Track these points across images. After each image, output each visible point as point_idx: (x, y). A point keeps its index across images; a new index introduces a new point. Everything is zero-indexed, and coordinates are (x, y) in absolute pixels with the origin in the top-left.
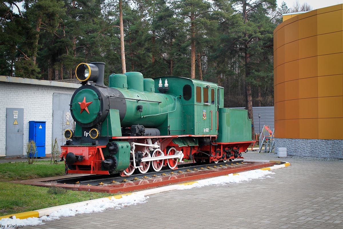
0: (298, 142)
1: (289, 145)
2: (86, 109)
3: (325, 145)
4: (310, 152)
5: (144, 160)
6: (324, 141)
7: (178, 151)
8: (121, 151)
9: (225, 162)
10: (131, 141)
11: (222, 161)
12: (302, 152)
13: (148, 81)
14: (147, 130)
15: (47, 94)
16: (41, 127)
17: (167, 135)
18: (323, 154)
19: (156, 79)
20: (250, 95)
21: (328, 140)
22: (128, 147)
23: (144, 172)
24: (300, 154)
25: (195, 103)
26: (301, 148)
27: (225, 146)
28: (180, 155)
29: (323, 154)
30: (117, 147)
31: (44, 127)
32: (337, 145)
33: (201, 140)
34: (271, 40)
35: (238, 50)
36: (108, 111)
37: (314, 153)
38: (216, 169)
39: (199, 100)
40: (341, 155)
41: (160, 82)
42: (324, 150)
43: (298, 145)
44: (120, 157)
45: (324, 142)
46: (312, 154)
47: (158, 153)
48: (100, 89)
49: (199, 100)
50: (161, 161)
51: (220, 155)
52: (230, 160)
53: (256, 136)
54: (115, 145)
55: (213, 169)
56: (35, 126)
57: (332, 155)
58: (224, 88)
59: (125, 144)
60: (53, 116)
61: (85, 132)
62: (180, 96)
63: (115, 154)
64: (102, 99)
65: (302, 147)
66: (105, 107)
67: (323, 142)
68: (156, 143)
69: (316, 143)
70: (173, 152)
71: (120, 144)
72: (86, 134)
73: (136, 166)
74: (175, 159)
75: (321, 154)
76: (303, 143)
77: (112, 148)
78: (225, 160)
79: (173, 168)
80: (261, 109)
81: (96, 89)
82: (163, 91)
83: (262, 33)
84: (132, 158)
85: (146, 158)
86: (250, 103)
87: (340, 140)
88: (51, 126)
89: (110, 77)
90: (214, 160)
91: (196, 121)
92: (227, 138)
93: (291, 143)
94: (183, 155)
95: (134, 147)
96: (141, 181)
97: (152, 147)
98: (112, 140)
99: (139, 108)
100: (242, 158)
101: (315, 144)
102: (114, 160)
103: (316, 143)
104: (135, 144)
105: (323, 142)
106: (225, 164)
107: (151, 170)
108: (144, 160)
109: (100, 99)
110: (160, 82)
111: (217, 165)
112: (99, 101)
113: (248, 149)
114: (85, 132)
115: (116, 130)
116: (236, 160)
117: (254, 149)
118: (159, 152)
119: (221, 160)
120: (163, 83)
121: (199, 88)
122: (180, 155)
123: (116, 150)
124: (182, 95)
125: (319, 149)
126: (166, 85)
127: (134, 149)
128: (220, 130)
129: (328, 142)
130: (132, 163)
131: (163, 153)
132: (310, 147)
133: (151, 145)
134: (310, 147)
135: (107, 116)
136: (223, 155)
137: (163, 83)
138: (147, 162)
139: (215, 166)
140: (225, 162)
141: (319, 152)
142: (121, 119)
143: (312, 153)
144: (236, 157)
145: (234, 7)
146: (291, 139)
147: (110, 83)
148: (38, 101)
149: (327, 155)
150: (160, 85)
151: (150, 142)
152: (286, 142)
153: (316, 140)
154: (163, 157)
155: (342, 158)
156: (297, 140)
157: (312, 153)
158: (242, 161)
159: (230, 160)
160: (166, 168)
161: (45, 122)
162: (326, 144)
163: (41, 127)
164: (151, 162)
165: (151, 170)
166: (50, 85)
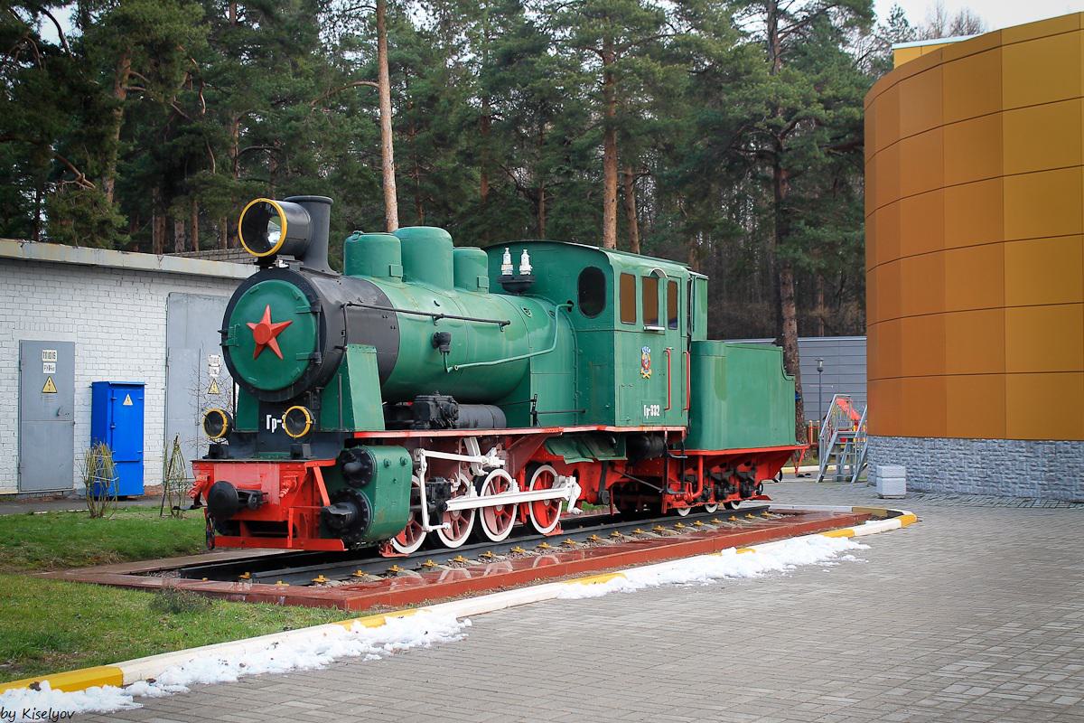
0: (941, 449)
1: (913, 458)
2: (273, 343)
3: (1028, 459)
4: (978, 479)
5: (455, 505)
6: (1024, 444)
7: (562, 478)
8: (382, 477)
9: (711, 510)
10: (412, 444)
11: (703, 509)
12: (956, 480)
13: (468, 257)
14: (465, 412)
15: (149, 297)
16: (128, 402)
17: (527, 425)
18: (1022, 485)
19: (494, 249)
20: (791, 298)
21: (1037, 441)
22: (403, 463)
23: (455, 544)
24: (948, 486)
25: (618, 325)
26: (950, 468)
27: (711, 461)
28: (569, 490)
29: (1022, 485)
30: (370, 465)
31: (139, 402)
32: (1066, 457)
33: (634, 442)
34: (858, 127)
35: (753, 159)
36: (340, 351)
37: (991, 484)
38: (683, 533)
39: (628, 316)
40: (1077, 490)
41: (507, 258)
42: (1024, 473)
43: (941, 458)
44: (380, 496)
45: (1024, 450)
46: (986, 486)
47: (500, 484)
48: (316, 281)
49: (628, 316)
50: (508, 508)
51: (695, 491)
52: (728, 506)
53: (808, 428)
54: (365, 458)
55: (674, 534)
56: (109, 397)
57: (1050, 489)
58: (706, 277)
59: (395, 456)
60: (167, 366)
61: (270, 416)
62: (570, 302)
63: (362, 486)
64: (322, 313)
65: (954, 465)
66: (333, 338)
67: (1020, 450)
68: (494, 451)
69: (998, 453)
70: (547, 481)
71: (379, 456)
72: (272, 423)
73: (431, 524)
74: (554, 503)
75: (1013, 486)
76: (957, 452)
77: (352, 466)
78: (712, 506)
79: (545, 531)
80: (824, 344)
81: (304, 281)
82: (514, 286)
83: (827, 104)
84: (416, 500)
85: (463, 498)
86: (790, 325)
87: (1073, 443)
88: (162, 397)
89: (348, 243)
90: (676, 505)
91: (618, 381)
92: (719, 437)
93: (920, 450)
94: (577, 491)
95: (424, 464)
96: (446, 571)
97: (480, 464)
98: (355, 443)
99: (439, 341)
100: (766, 498)
101: (995, 453)
102: (360, 505)
103: (998, 453)
104: (425, 453)
105: (1022, 447)
106: (710, 518)
107: (478, 536)
108: (455, 505)
109: (315, 313)
110: (507, 258)
111: (685, 520)
112: (312, 318)
113: (784, 470)
114: (269, 416)
115: (367, 411)
116: (745, 504)
117: (802, 469)
118: (504, 480)
119: (700, 504)
120: (516, 262)
121: (628, 279)
122: (569, 490)
123: (366, 475)
124: (575, 300)
125: (1008, 469)
126: (526, 267)
127: (424, 470)
128: (695, 410)
129: (1036, 447)
130: (418, 516)
131: (515, 484)
132: (978, 466)
133: (476, 457)
134: (978, 466)
135: (339, 365)
136: (705, 489)
137: (516, 262)
138: (465, 513)
139: (680, 525)
140: (711, 510)
141: (1009, 481)
142: (384, 375)
143: (986, 484)
144: (745, 495)
145: (741, 23)
146: (919, 438)
147: (346, 263)
148: (119, 319)
149: (1035, 491)
150: (507, 268)
151: (474, 447)
152: (904, 450)
153: (1000, 441)
154: (514, 495)
155: (1080, 498)
156: (939, 443)
157: (986, 484)
158: (766, 508)
159: (728, 506)
160: (524, 531)
161: (141, 387)
162: (1029, 455)
163: (128, 402)
164: (478, 510)
165: (478, 536)
166: (157, 268)
